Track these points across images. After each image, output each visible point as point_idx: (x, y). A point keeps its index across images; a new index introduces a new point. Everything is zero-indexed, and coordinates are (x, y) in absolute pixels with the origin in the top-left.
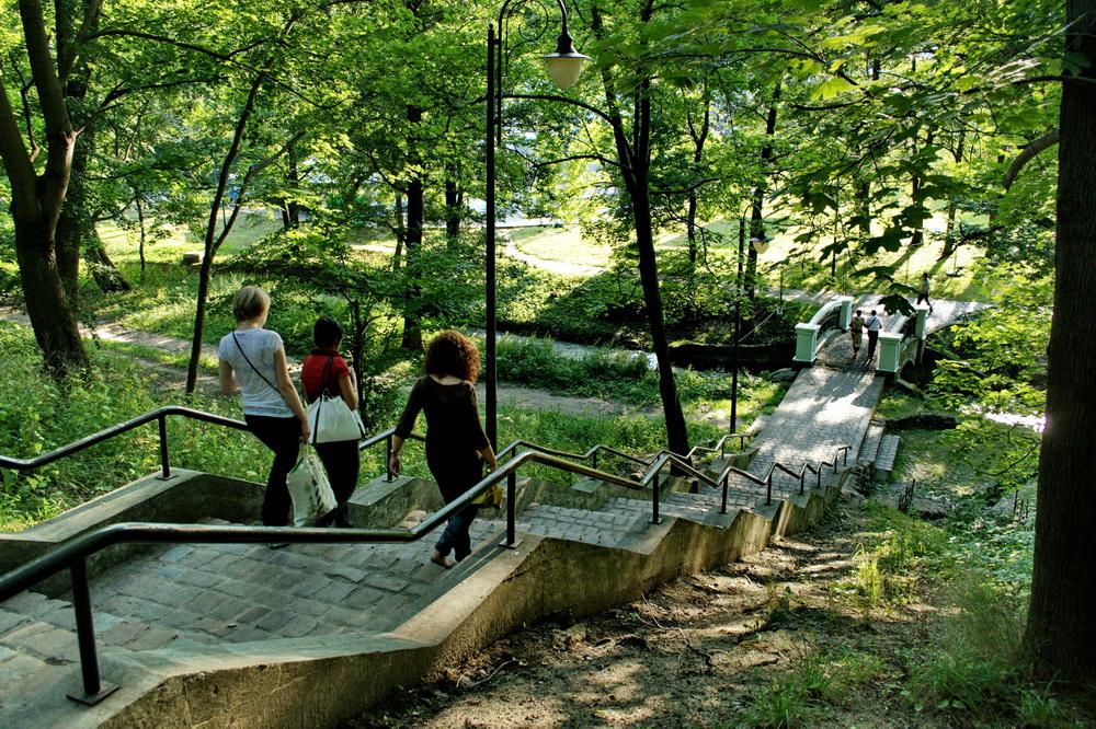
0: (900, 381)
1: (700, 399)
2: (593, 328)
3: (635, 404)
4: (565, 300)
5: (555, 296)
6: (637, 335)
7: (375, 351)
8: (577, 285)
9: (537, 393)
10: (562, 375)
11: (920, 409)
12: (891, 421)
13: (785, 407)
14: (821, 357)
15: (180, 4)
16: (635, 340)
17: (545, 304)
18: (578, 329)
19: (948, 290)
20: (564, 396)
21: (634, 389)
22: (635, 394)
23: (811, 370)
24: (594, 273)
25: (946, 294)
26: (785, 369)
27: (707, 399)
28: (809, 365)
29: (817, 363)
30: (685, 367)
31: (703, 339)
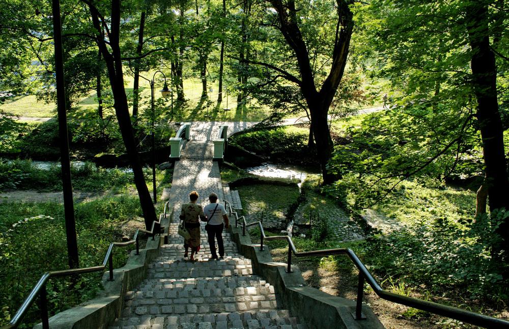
0: (225, 162)
1: (128, 185)
2: (48, 151)
3: (90, 191)
4: (28, 137)
5: (22, 135)
6: (74, 153)
7: (226, 295)
8: (34, 128)
9: (28, 192)
10: (42, 180)
11: (239, 175)
12: (230, 183)
13: (177, 182)
14: (183, 154)
15: (447, 2)
16: (74, 156)
17: (16, 140)
18: (40, 152)
19: (227, 117)
20: (46, 192)
21: (87, 183)
22: (89, 186)
23: (180, 161)
24: (285, 177)
25: (228, 119)
26: (165, 163)
27: (131, 184)
28: (178, 159)
29: (183, 158)
30: (114, 167)
31: (113, 152)
